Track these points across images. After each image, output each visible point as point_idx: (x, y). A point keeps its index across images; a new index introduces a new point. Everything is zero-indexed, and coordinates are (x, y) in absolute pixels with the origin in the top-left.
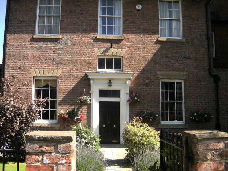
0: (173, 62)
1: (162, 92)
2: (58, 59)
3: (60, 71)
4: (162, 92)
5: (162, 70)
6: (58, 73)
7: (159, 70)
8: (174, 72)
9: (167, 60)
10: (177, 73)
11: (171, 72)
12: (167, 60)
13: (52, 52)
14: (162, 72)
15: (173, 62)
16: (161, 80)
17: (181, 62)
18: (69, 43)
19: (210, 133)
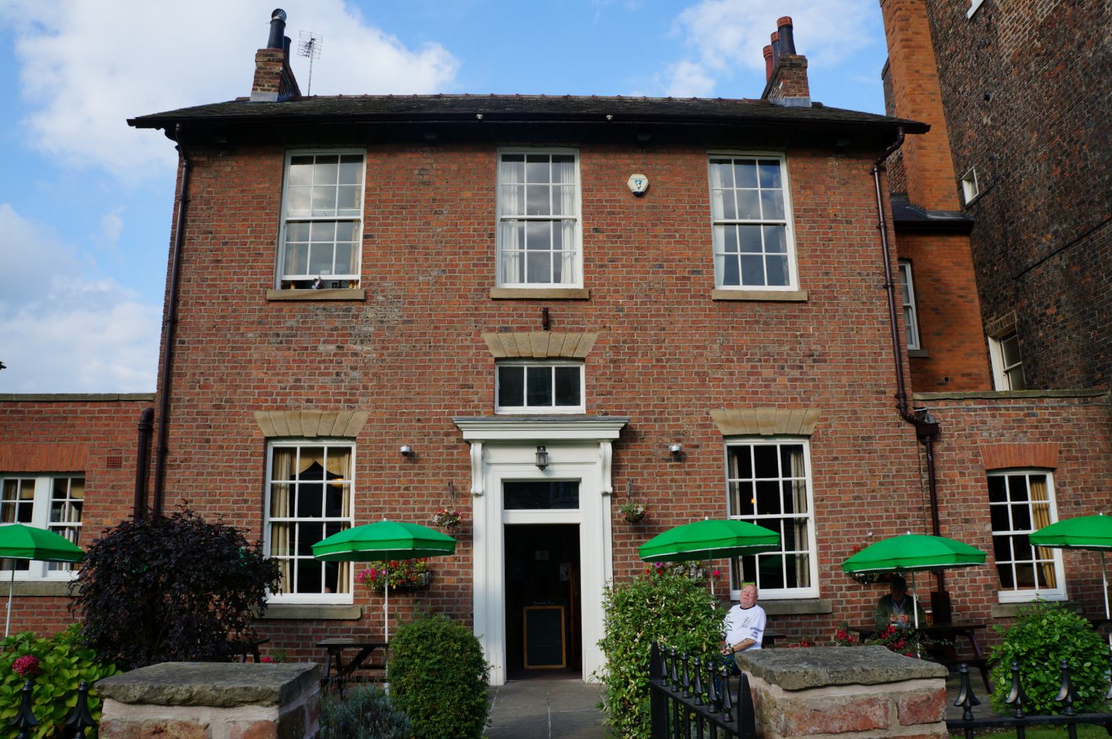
0: (767, 373)
5: (730, 406)
10: (786, 412)
11: (760, 412)
12: (747, 366)
15: (767, 373)
18: (394, 315)
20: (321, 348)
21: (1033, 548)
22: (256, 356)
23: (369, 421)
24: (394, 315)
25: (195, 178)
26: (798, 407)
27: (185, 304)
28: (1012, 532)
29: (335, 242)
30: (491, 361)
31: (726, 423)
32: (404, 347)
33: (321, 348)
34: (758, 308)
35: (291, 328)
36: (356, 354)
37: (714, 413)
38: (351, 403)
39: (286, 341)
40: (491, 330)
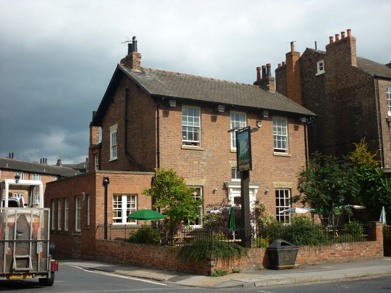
0: (283, 173)
1: (236, 238)
2: (202, 170)
3: (205, 180)
4: (236, 238)
5: (277, 181)
6: (203, 182)
7: (274, 181)
8: (284, 182)
9: (279, 172)
10: (286, 183)
11: (283, 182)
12: (279, 172)
13: (197, 162)
14: (277, 182)
15: (283, 173)
16: (13, 268)
17: (288, 174)
18: (210, 155)
19: (274, 78)
20: (195, 162)
21: (2, 202)
22: (180, 164)
23: (206, 182)
24: (210, 155)
25: (238, 136)
26: (289, 182)
27: (161, 148)
28: (280, 207)
29: (193, 132)
30: (231, 167)
31: (276, 185)
32: (213, 163)
33: (195, 162)
34: (129, 108)
35: (187, 157)
36: (202, 164)
37: (274, 183)
38: (202, 177)
39: (186, 160)
40: (230, 160)
